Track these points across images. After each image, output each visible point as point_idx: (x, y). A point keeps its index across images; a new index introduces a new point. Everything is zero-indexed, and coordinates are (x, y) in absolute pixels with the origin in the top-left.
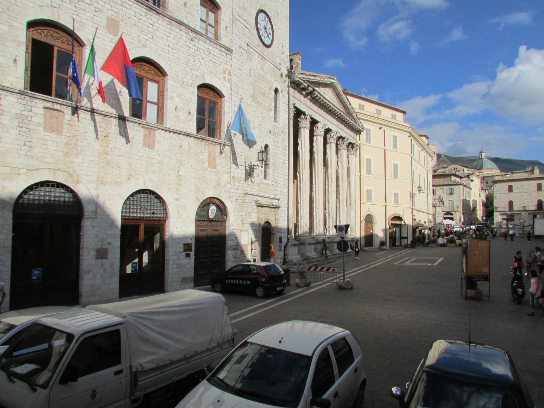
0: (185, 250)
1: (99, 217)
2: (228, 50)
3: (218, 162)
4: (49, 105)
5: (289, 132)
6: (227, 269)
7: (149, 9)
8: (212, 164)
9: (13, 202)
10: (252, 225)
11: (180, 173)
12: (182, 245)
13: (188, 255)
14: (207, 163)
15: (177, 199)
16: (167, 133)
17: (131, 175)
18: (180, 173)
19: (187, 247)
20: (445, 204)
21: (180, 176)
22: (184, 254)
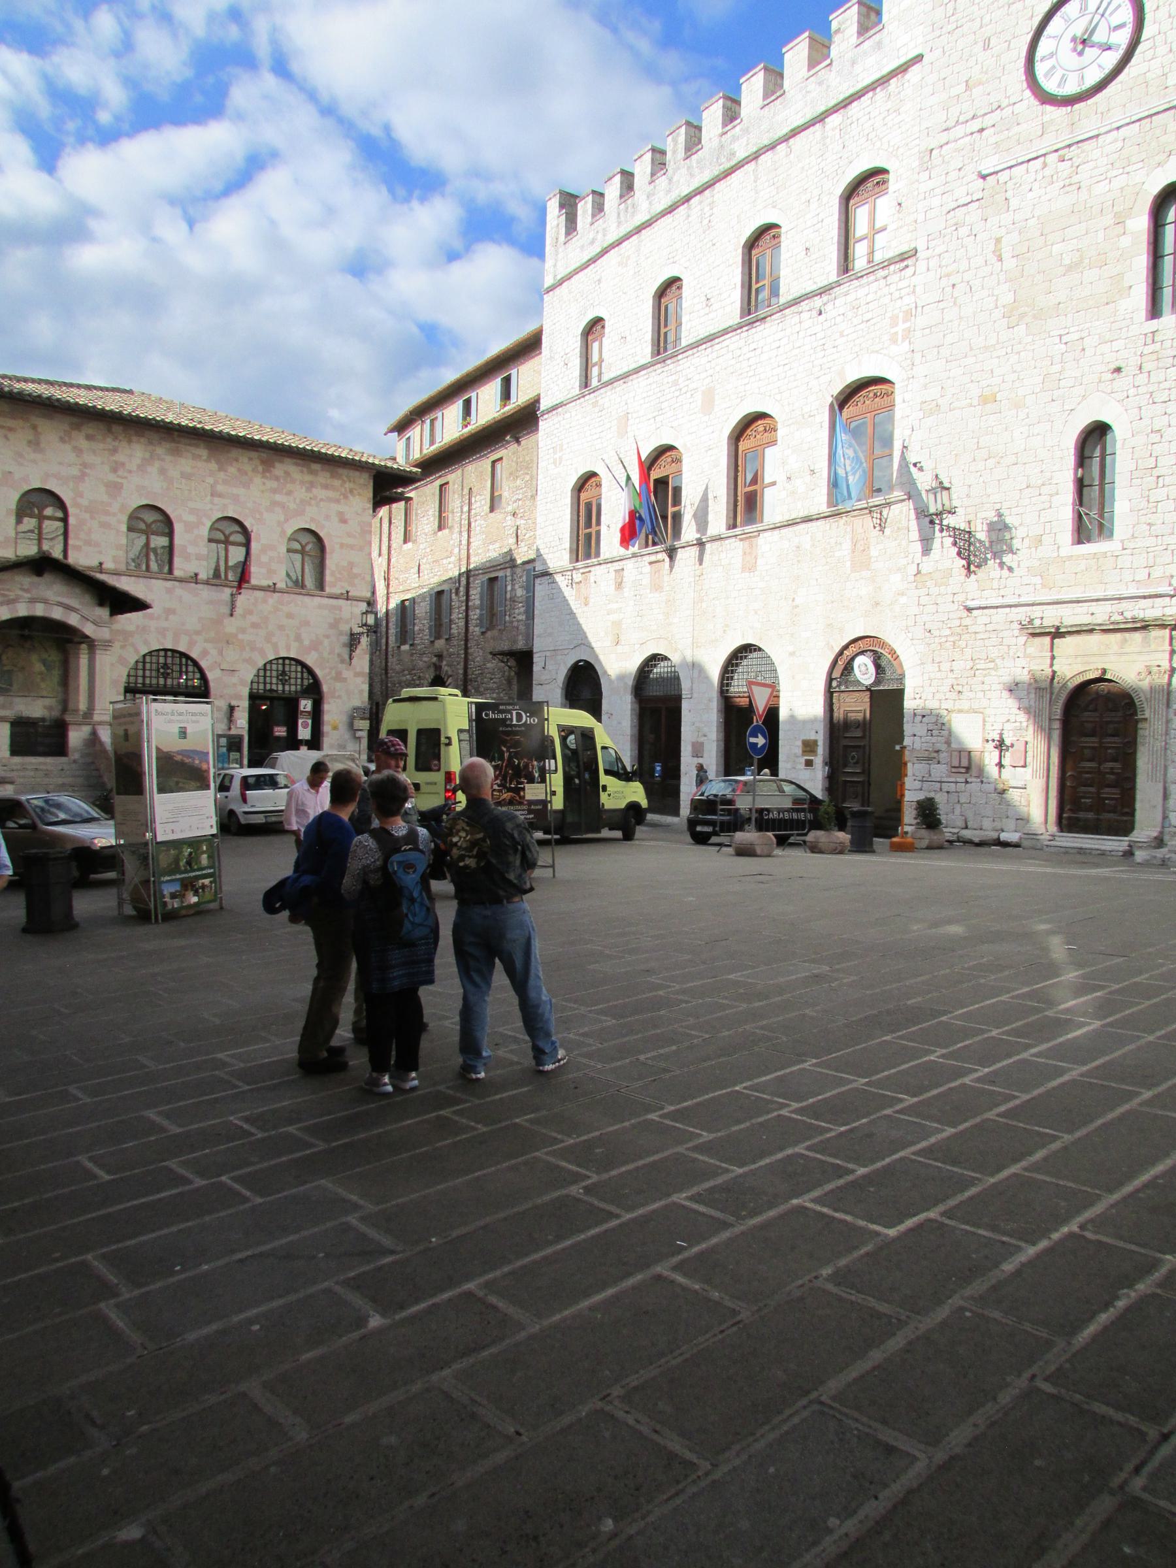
0: (805, 752)
1: (695, 695)
2: (903, 257)
3: (874, 552)
4: (653, 558)
5: (390, 540)
6: (135, 913)
7: (709, 344)
8: (861, 558)
9: (630, 682)
10: (1013, 688)
11: (797, 602)
12: (799, 743)
13: (809, 763)
14: (848, 564)
15: (792, 654)
16: (776, 532)
17: (727, 626)
18: (797, 602)
19: (809, 747)
20: (458, 270)
21: (797, 606)
22: (803, 760)
